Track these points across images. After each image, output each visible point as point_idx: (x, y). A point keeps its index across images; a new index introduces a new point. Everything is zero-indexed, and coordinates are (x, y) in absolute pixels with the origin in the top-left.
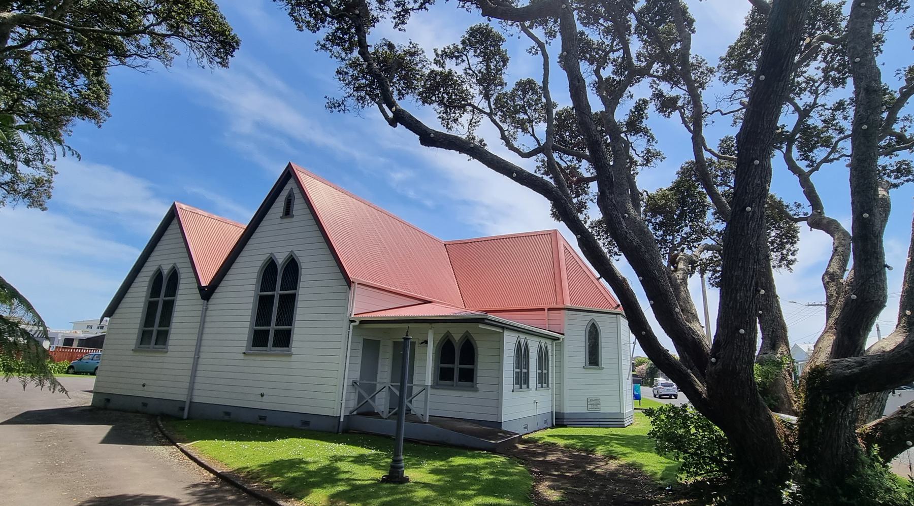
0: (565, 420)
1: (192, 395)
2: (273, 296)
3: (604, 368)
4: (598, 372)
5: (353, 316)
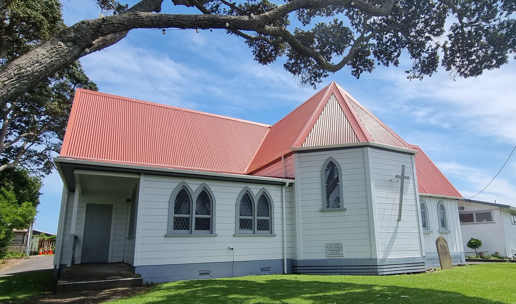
0: (378, 267)
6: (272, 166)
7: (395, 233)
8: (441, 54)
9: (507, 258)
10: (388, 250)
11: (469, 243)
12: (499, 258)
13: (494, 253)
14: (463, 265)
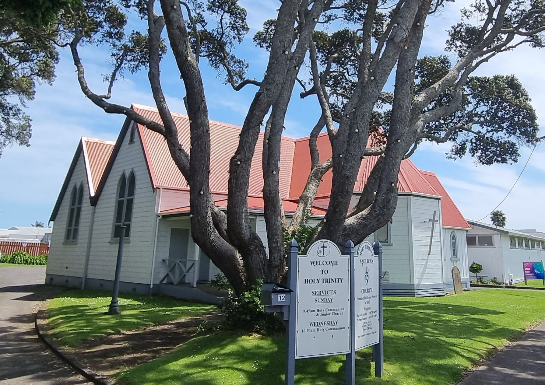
0: (415, 291)
2: (123, 201)
5: (159, 212)
6: (321, 200)
7: (426, 264)
8: (468, 146)
9: (504, 284)
10: (421, 279)
11: (471, 267)
12: (497, 283)
14: (468, 290)
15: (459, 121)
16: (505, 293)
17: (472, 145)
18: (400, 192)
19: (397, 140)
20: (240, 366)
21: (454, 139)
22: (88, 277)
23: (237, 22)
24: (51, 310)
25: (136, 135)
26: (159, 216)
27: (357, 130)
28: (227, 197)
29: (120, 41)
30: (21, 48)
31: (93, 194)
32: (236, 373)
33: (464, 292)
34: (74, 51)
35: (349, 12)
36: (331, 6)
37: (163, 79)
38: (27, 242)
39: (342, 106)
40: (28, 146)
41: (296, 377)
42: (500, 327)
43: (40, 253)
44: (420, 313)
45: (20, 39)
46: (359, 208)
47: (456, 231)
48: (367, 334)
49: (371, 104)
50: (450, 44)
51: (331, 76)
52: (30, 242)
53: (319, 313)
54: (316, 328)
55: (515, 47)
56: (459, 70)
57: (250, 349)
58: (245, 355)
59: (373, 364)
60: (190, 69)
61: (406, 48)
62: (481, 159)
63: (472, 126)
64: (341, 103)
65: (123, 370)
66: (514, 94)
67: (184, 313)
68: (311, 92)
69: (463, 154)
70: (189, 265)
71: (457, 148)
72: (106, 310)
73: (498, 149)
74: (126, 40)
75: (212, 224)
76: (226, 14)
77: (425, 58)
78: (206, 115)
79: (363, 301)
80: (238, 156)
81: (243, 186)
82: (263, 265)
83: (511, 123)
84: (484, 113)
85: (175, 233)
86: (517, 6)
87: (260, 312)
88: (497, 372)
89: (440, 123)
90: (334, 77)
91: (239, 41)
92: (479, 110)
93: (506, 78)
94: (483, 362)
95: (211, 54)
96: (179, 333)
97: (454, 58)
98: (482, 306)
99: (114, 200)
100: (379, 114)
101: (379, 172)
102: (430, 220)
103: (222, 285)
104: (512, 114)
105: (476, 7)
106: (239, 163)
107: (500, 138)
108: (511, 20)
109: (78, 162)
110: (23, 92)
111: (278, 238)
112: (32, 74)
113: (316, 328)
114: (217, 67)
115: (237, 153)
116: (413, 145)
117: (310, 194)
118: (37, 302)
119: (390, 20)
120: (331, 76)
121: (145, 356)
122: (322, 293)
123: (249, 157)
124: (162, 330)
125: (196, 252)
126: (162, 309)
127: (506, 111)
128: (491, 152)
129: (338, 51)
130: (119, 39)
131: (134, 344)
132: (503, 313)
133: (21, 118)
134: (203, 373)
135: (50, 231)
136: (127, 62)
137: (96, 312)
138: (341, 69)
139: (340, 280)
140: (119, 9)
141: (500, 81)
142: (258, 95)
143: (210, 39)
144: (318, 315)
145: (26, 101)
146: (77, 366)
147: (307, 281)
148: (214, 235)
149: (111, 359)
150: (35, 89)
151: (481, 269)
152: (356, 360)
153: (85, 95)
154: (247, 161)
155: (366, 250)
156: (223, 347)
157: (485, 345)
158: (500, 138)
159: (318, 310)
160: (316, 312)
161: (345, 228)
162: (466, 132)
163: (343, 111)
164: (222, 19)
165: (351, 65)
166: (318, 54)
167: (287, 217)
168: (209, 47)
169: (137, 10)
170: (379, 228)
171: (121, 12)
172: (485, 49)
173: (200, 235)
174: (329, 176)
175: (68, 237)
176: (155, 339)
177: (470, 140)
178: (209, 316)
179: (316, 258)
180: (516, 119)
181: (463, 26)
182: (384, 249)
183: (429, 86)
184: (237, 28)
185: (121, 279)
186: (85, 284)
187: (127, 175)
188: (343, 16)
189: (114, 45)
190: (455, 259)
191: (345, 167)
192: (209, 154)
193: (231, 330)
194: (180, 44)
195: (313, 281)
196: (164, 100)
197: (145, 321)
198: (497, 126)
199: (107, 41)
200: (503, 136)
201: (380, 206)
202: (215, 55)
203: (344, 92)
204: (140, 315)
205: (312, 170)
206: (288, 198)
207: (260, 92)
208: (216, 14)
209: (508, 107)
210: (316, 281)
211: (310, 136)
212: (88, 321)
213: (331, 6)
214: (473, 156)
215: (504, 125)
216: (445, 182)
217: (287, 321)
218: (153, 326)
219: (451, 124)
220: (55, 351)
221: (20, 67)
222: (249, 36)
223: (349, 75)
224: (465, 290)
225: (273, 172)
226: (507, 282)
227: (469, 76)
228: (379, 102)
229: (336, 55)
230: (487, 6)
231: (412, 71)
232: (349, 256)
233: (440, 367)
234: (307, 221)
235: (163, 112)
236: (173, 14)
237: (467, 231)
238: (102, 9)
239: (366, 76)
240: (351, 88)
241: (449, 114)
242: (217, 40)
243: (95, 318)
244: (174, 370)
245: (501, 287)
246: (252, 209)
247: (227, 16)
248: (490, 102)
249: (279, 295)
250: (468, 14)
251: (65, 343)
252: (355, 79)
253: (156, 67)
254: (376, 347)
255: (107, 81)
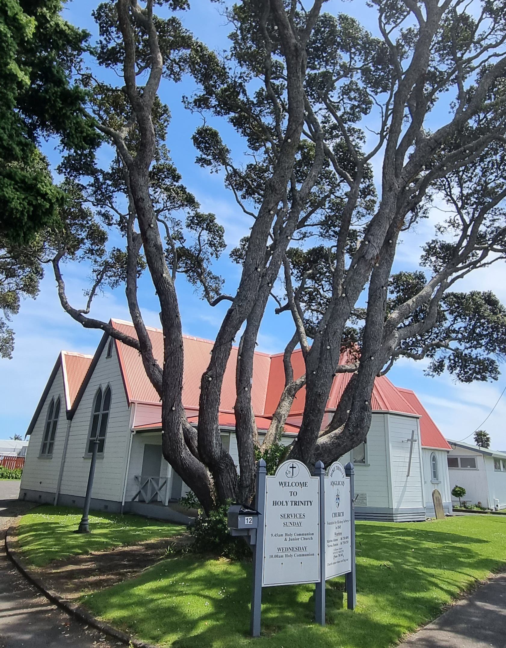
0: (394, 515)
1: (60, 489)
2: (98, 415)
3: (369, 465)
4: (365, 468)
5: (133, 427)
7: (405, 486)
10: (399, 502)
11: (454, 490)
12: (481, 508)
13: (477, 504)
15: (436, 337)
16: (490, 520)
17: (450, 361)
18: (373, 410)
19: (371, 357)
20: (206, 593)
21: (432, 356)
22: (61, 493)
23: (215, 239)
24: (22, 527)
25: (114, 349)
26: (133, 432)
27: (329, 347)
28: (198, 412)
29: (101, 257)
30: (8, 264)
31: (69, 408)
32: (202, 600)
33: (446, 518)
34: (56, 267)
35: (324, 229)
36: (306, 224)
37: (140, 295)
38: (4, 455)
39: (317, 321)
40: (11, 358)
41: (263, 606)
42: (483, 558)
43: (16, 467)
44: (398, 540)
45: (9, 255)
46: (332, 427)
47: (436, 452)
48: (338, 562)
49: (342, 320)
50: (425, 258)
51: (305, 292)
52: (7, 455)
53: (288, 538)
54: (284, 554)
55: (490, 263)
56: (433, 287)
57: (218, 575)
58: (213, 582)
59: (345, 595)
60: (165, 285)
61: (377, 265)
62: (460, 377)
63: (449, 343)
64: (316, 319)
65: (87, 593)
66: (492, 311)
67: (154, 533)
68: (286, 308)
69: (441, 371)
70: (161, 482)
71: (435, 365)
72: (76, 528)
73: (477, 366)
74: (107, 257)
75: (183, 441)
76: (205, 231)
77: (400, 274)
78: (180, 331)
79: (334, 526)
80: (210, 372)
81: (215, 403)
82: (233, 484)
83: (490, 340)
84: (462, 329)
85: (147, 448)
86: (492, 223)
87: (229, 534)
88: (478, 608)
89: (416, 339)
90: (308, 293)
91: (217, 257)
92: (456, 327)
93: (483, 294)
94: (463, 596)
95: (189, 270)
96: (147, 555)
97: (429, 273)
98: (464, 534)
99: (90, 414)
100: (354, 330)
101: (352, 389)
102: (408, 440)
103: (193, 503)
104: (490, 330)
105: (450, 222)
106: (210, 379)
107: (478, 355)
108: (485, 237)
109: (57, 376)
110: (8, 306)
111: (250, 456)
112: (17, 289)
113: (284, 554)
114: (195, 283)
115: (209, 369)
116: (389, 362)
117: (284, 410)
118: (9, 518)
119: (364, 235)
120: (305, 292)
121: (111, 579)
122: (290, 516)
123: (220, 373)
124: (130, 551)
125: (169, 471)
126: (132, 528)
127: (484, 327)
128: (470, 369)
129: (313, 266)
130: (100, 255)
131: (100, 565)
132: (487, 542)
133: (5, 331)
134: (168, 599)
135: (26, 444)
136: (107, 278)
137: (66, 530)
138: (317, 285)
139: (309, 503)
140: (101, 227)
141: (477, 297)
142: (230, 312)
143: (189, 256)
144: (286, 540)
145: (10, 315)
146: (42, 587)
147: (275, 503)
148: (186, 453)
149: (76, 580)
150: (19, 304)
151: (464, 493)
152: (327, 590)
153: (64, 310)
154: (219, 377)
155: (337, 471)
156: (190, 571)
157: (466, 577)
158: (478, 355)
159: (286, 535)
160: (284, 537)
161: (318, 447)
162: (444, 348)
163: (317, 326)
164: (200, 236)
165: (326, 281)
166: (293, 270)
167: (260, 434)
168: (187, 263)
169: (119, 228)
170: (352, 448)
171: (103, 229)
172: (460, 265)
173: (170, 452)
174: (302, 393)
175: (43, 451)
176: (123, 560)
177: (448, 356)
178: (179, 537)
179: (285, 479)
180: (495, 336)
181: (437, 243)
182: (356, 470)
183: (405, 302)
184: (214, 244)
185: (93, 495)
186: (58, 500)
187: (103, 389)
188: (318, 233)
189: (95, 261)
190: (436, 482)
191: (317, 385)
192: (182, 370)
193: (200, 553)
194: (156, 260)
195: (282, 503)
196: (140, 315)
197: (114, 541)
198: (475, 343)
199: (88, 258)
200: (482, 353)
201: (353, 425)
202: (192, 271)
203: (319, 308)
204: (110, 534)
205: (286, 386)
206: (263, 414)
207: (233, 308)
208: (195, 231)
209: (486, 323)
210: (285, 503)
211: (284, 352)
212: (58, 539)
213: (306, 224)
214: (451, 373)
215: (483, 342)
216: (423, 399)
217: (255, 546)
218: (122, 547)
219: (428, 340)
220: (21, 571)
221: (6, 282)
222: (226, 252)
223: (324, 291)
224: (447, 516)
225: (244, 388)
226: (492, 507)
227: (444, 293)
228: (354, 317)
229: (311, 271)
230: (461, 223)
231: (385, 288)
232: (319, 477)
233: (416, 600)
234: (280, 439)
235: (138, 326)
236: (150, 233)
237: (448, 452)
238: (84, 227)
239: (340, 292)
240: (326, 304)
241: (425, 330)
242: (195, 256)
243: (65, 536)
244: (138, 595)
245: (486, 513)
246: (226, 425)
247: (205, 232)
248: (468, 318)
249: (246, 518)
250: (442, 229)
251: (31, 562)
252: (329, 295)
253: (134, 282)
254: (348, 576)
255: (87, 296)
